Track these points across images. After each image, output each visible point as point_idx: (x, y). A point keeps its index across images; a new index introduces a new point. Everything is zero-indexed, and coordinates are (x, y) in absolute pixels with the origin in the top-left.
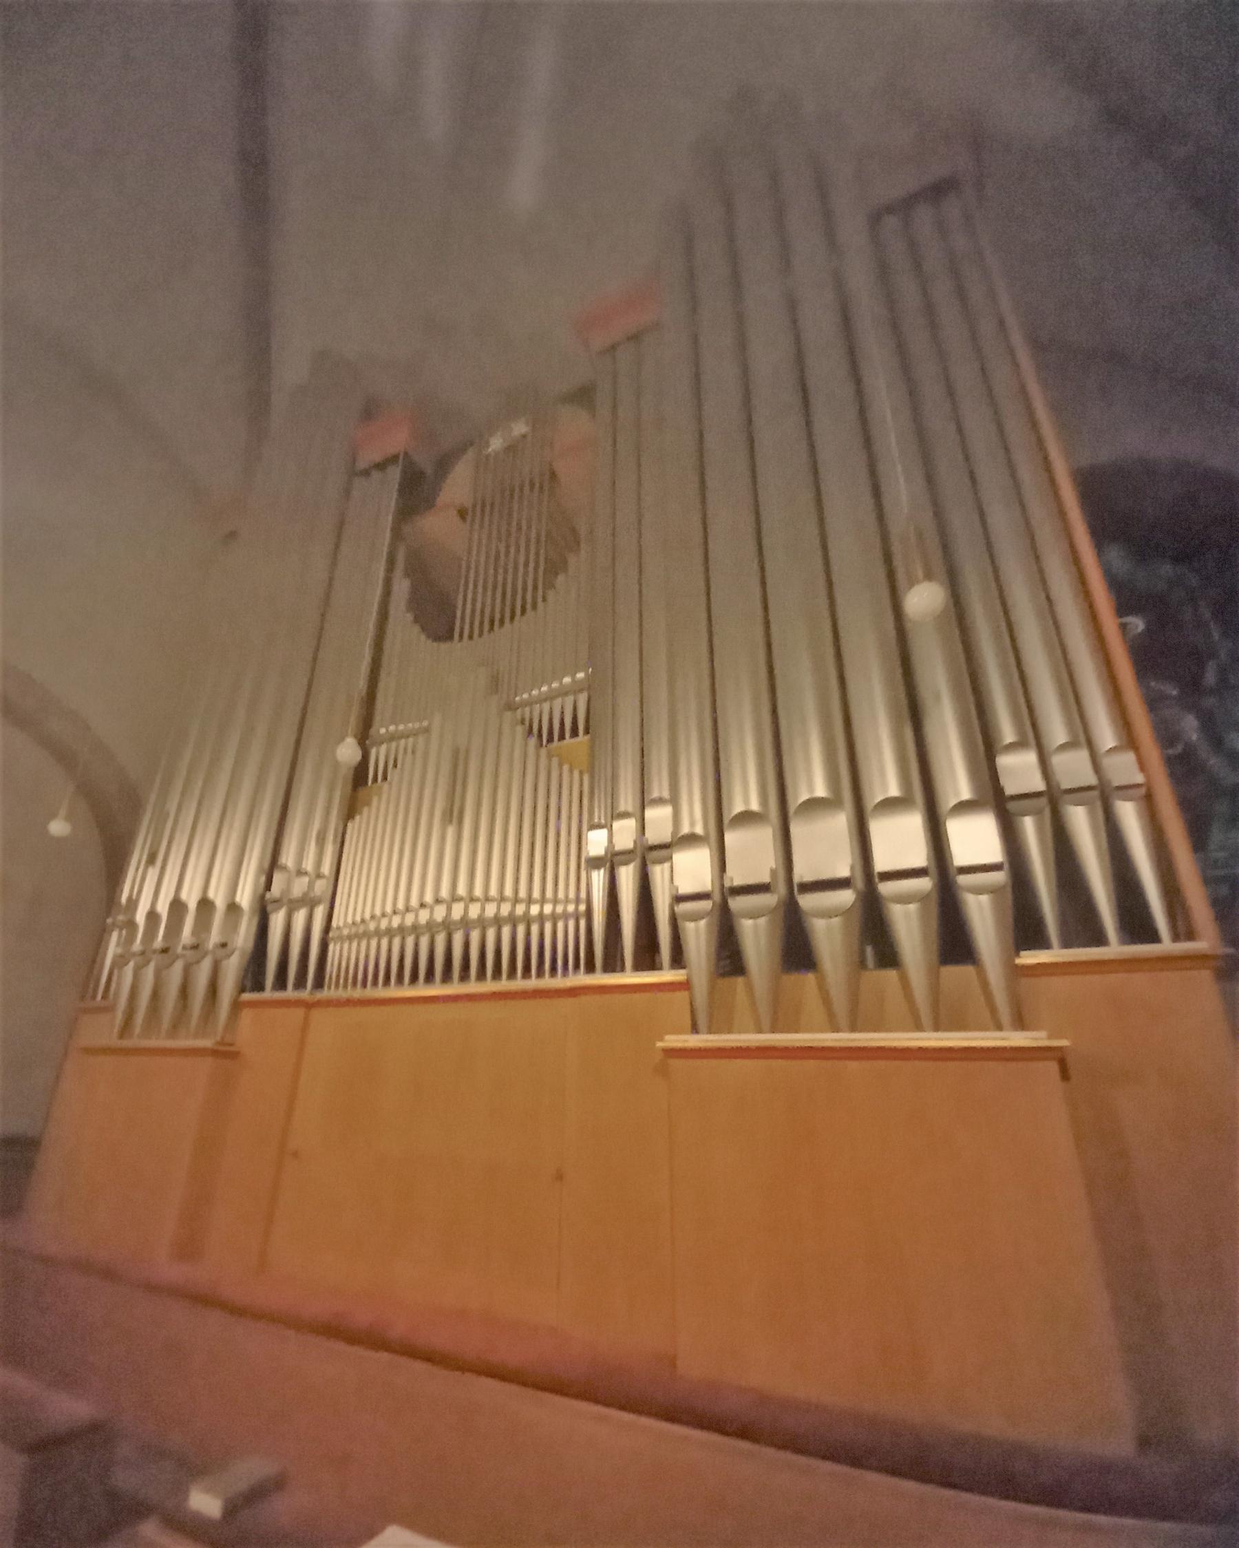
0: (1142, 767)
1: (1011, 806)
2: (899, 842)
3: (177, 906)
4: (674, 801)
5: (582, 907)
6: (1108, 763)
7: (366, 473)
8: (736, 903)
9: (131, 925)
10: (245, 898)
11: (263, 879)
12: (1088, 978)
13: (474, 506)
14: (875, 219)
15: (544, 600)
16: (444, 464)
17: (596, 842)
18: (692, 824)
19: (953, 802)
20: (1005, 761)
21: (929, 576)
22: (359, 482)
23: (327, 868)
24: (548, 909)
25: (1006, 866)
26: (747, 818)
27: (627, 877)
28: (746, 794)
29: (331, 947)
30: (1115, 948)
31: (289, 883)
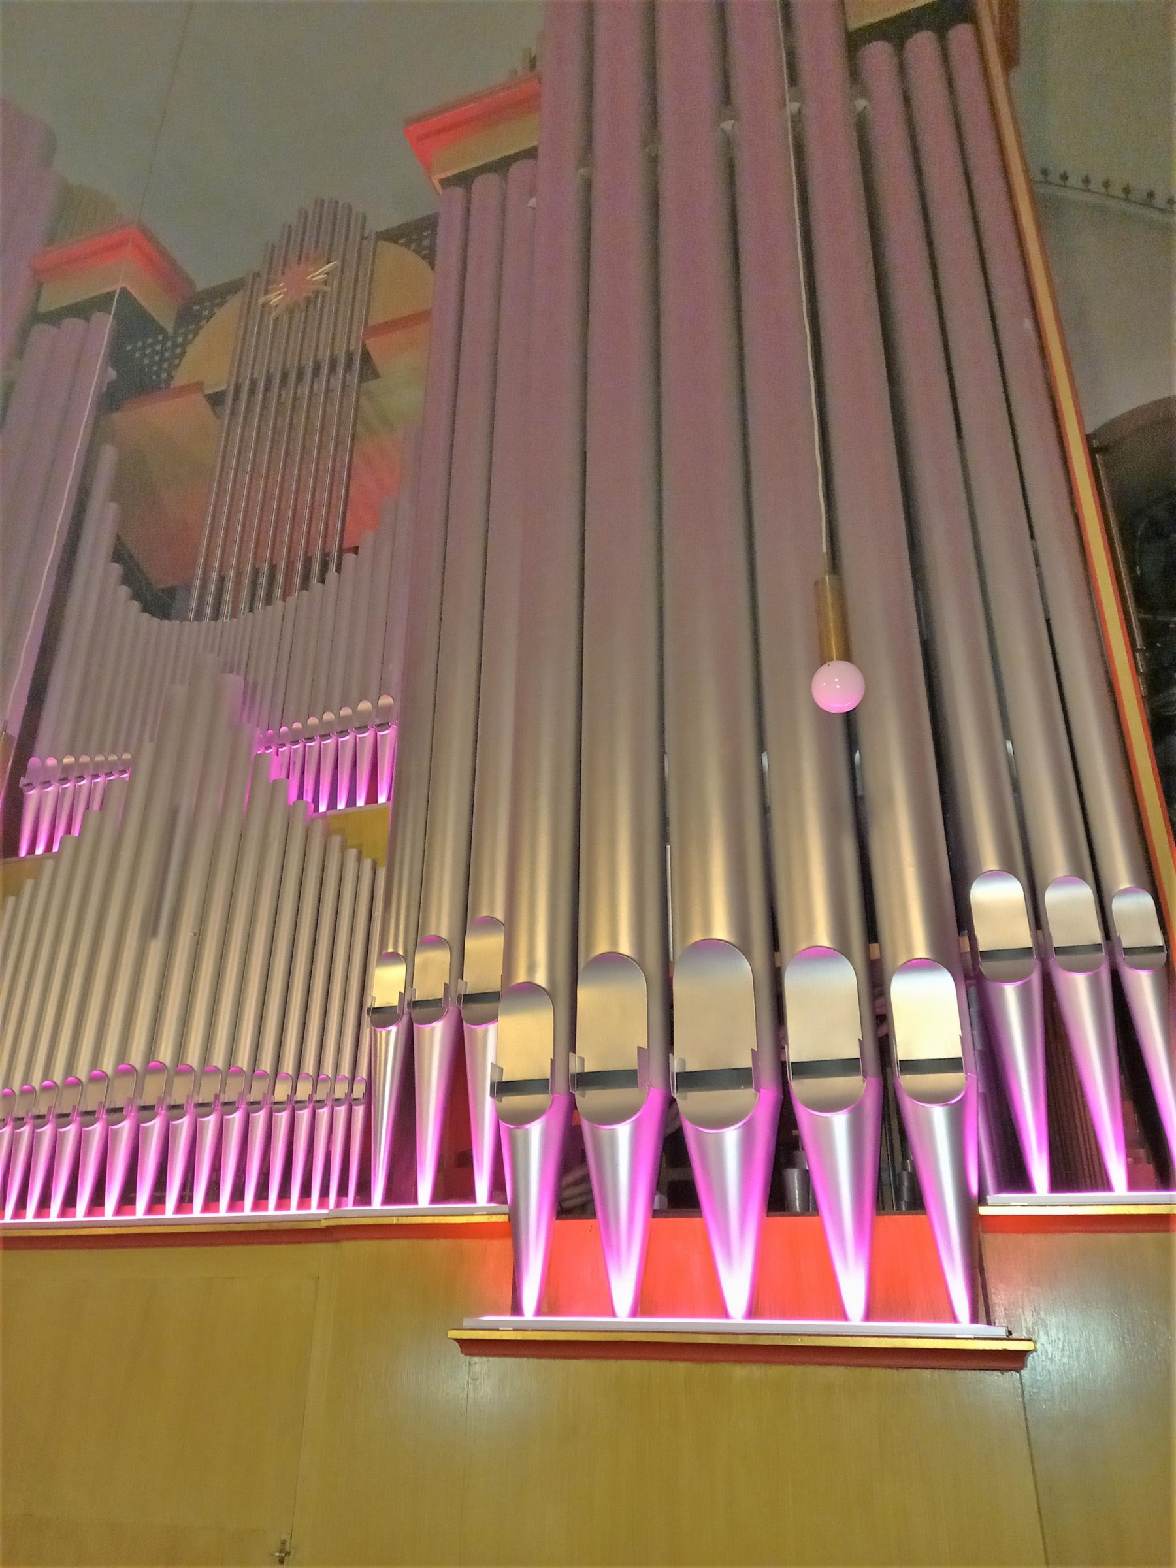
1: (986, 967)
4: (509, 928)
5: (359, 1090)
7: (54, 318)
12: (1113, 1237)
13: (238, 389)
14: (855, 41)
15: (338, 570)
17: (388, 985)
19: (902, 959)
22: (42, 334)
24: (304, 1091)
25: (897, 1068)
27: (435, 1039)
30: (1120, 1195)
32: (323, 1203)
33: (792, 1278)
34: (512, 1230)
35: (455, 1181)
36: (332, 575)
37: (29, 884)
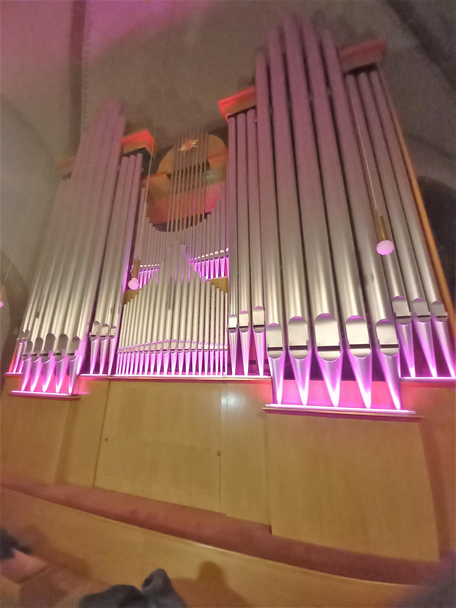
0: (446, 310)
2: (358, 334)
3: (50, 336)
5: (226, 347)
6: (434, 308)
7: (128, 155)
8: (292, 353)
9: (30, 343)
10: (81, 334)
11: (88, 327)
14: (344, 76)
16: (160, 154)
17: (233, 323)
18: (274, 320)
19: (378, 320)
20: (396, 304)
21: (387, 239)
22: (125, 159)
23: (116, 324)
26: (296, 320)
28: (296, 309)
29: (119, 355)
31: (100, 330)
32: (121, 373)
33: (347, 397)
34: (273, 383)
35: (253, 370)
36: (204, 220)
37: (136, 296)
